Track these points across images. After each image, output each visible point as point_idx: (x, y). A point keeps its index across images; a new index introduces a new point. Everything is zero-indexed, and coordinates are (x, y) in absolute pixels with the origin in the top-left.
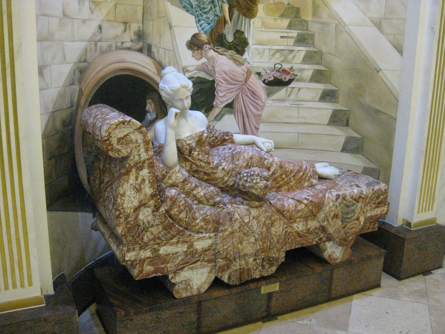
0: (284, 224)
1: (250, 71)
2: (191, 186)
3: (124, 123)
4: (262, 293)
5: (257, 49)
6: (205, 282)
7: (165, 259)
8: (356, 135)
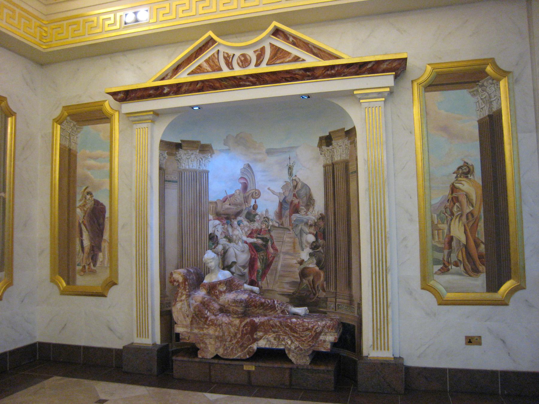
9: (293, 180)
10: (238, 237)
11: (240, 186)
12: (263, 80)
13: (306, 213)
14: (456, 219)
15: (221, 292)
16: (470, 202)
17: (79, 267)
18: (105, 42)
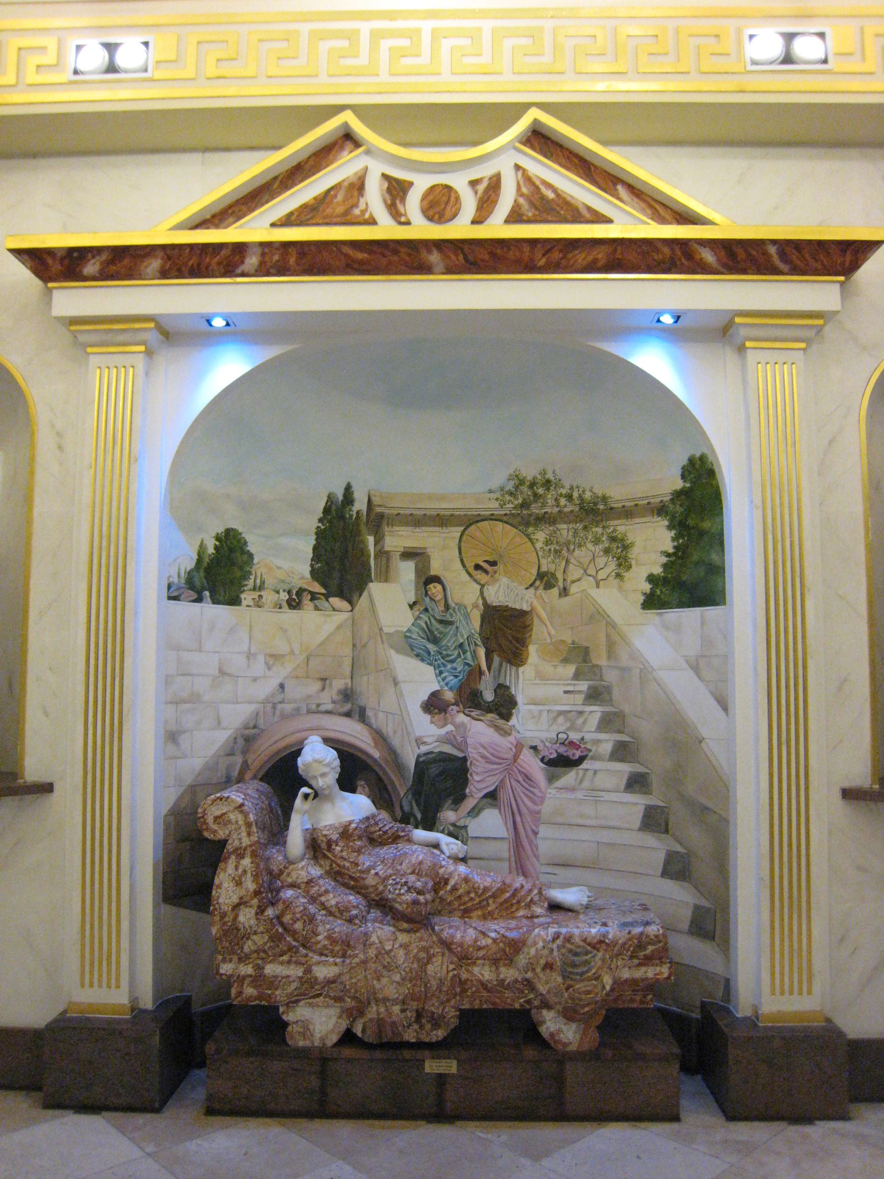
0: (452, 963)
1: (521, 743)
2: (319, 890)
3: (221, 799)
4: (426, 1071)
5: (530, 711)
6: (333, 1031)
7: (273, 982)
8: (679, 848)
18: (115, 114)
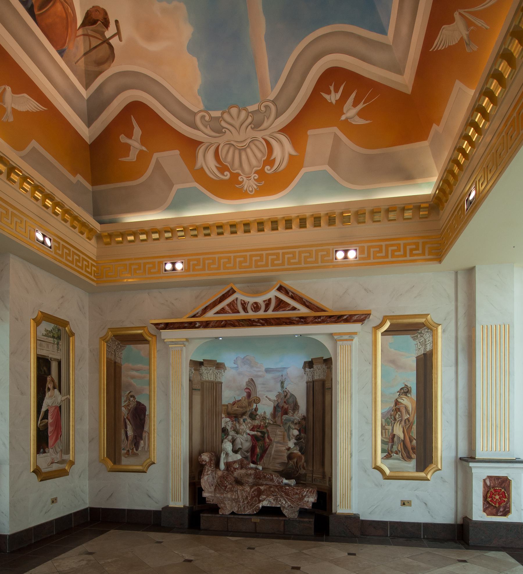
9: (284, 391)
10: (243, 430)
11: (245, 394)
12: (270, 323)
13: (293, 415)
14: (397, 423)
15: (235, 469)
16: (407, 412)
17: (124, 451)
